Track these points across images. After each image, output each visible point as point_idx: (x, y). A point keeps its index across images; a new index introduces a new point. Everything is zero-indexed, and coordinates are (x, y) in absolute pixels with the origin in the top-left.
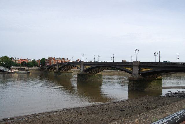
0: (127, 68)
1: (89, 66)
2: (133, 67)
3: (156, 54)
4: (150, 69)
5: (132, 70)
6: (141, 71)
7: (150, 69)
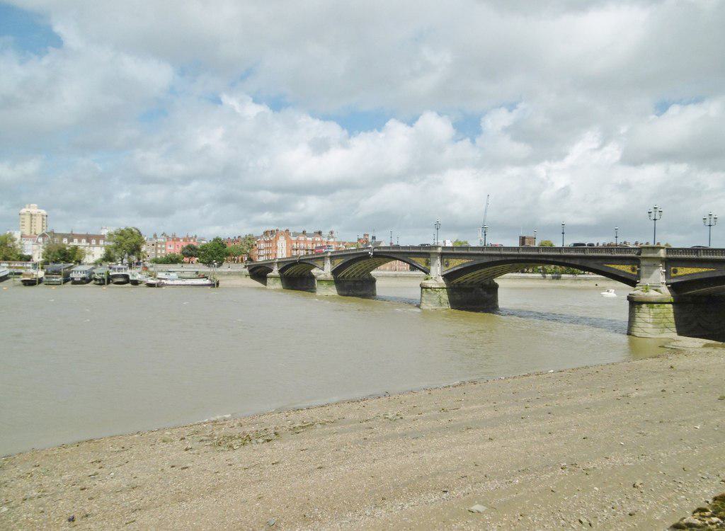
4: (704, 270)
5: (636, 273)
7: (704, 270)
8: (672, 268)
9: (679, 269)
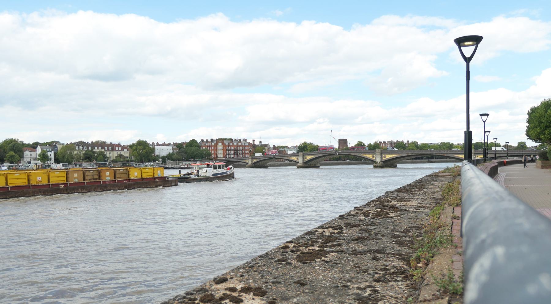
0: (459, 156)
1: (313, 156)
2: (376, 154)
9: (479, 156)
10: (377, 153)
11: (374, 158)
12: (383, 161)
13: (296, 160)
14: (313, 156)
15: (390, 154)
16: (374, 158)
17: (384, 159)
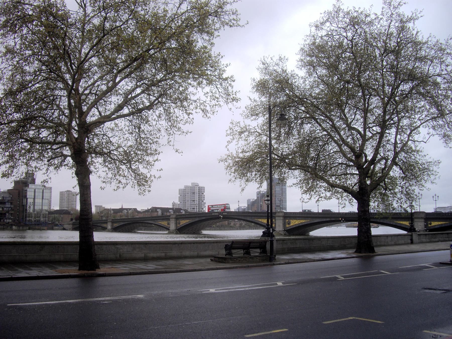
1: (188, 221)
3: (437, 198)
4: (444, 223)
6: (429, 226)
7: (444, 223)
8: (429, 222)
10: (171, 218)
11: (169, 226)
12: (286, 229)
13: (167, 225)
14: (304, 221)
15: (298, 218)
16: (169, 226)
17: (287, 226)
